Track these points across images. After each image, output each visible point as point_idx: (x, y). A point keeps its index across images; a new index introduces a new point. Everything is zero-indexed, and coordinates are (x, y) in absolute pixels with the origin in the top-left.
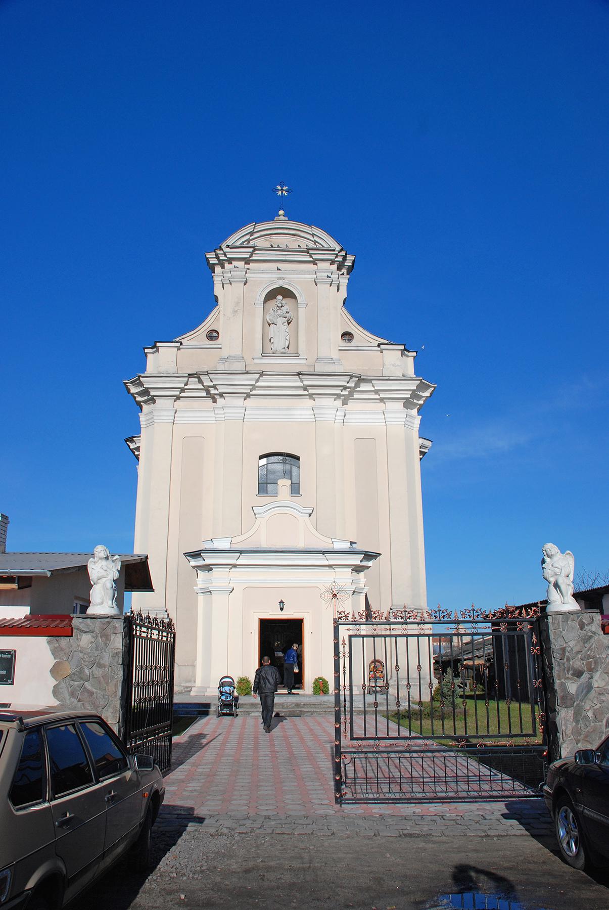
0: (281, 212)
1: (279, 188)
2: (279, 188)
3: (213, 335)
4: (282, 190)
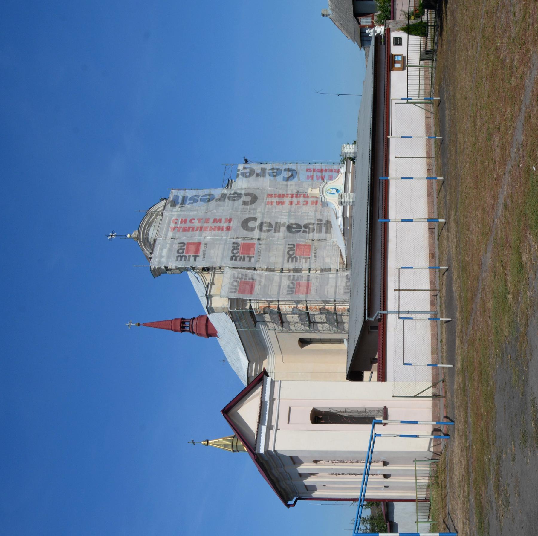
4: (112, 236)
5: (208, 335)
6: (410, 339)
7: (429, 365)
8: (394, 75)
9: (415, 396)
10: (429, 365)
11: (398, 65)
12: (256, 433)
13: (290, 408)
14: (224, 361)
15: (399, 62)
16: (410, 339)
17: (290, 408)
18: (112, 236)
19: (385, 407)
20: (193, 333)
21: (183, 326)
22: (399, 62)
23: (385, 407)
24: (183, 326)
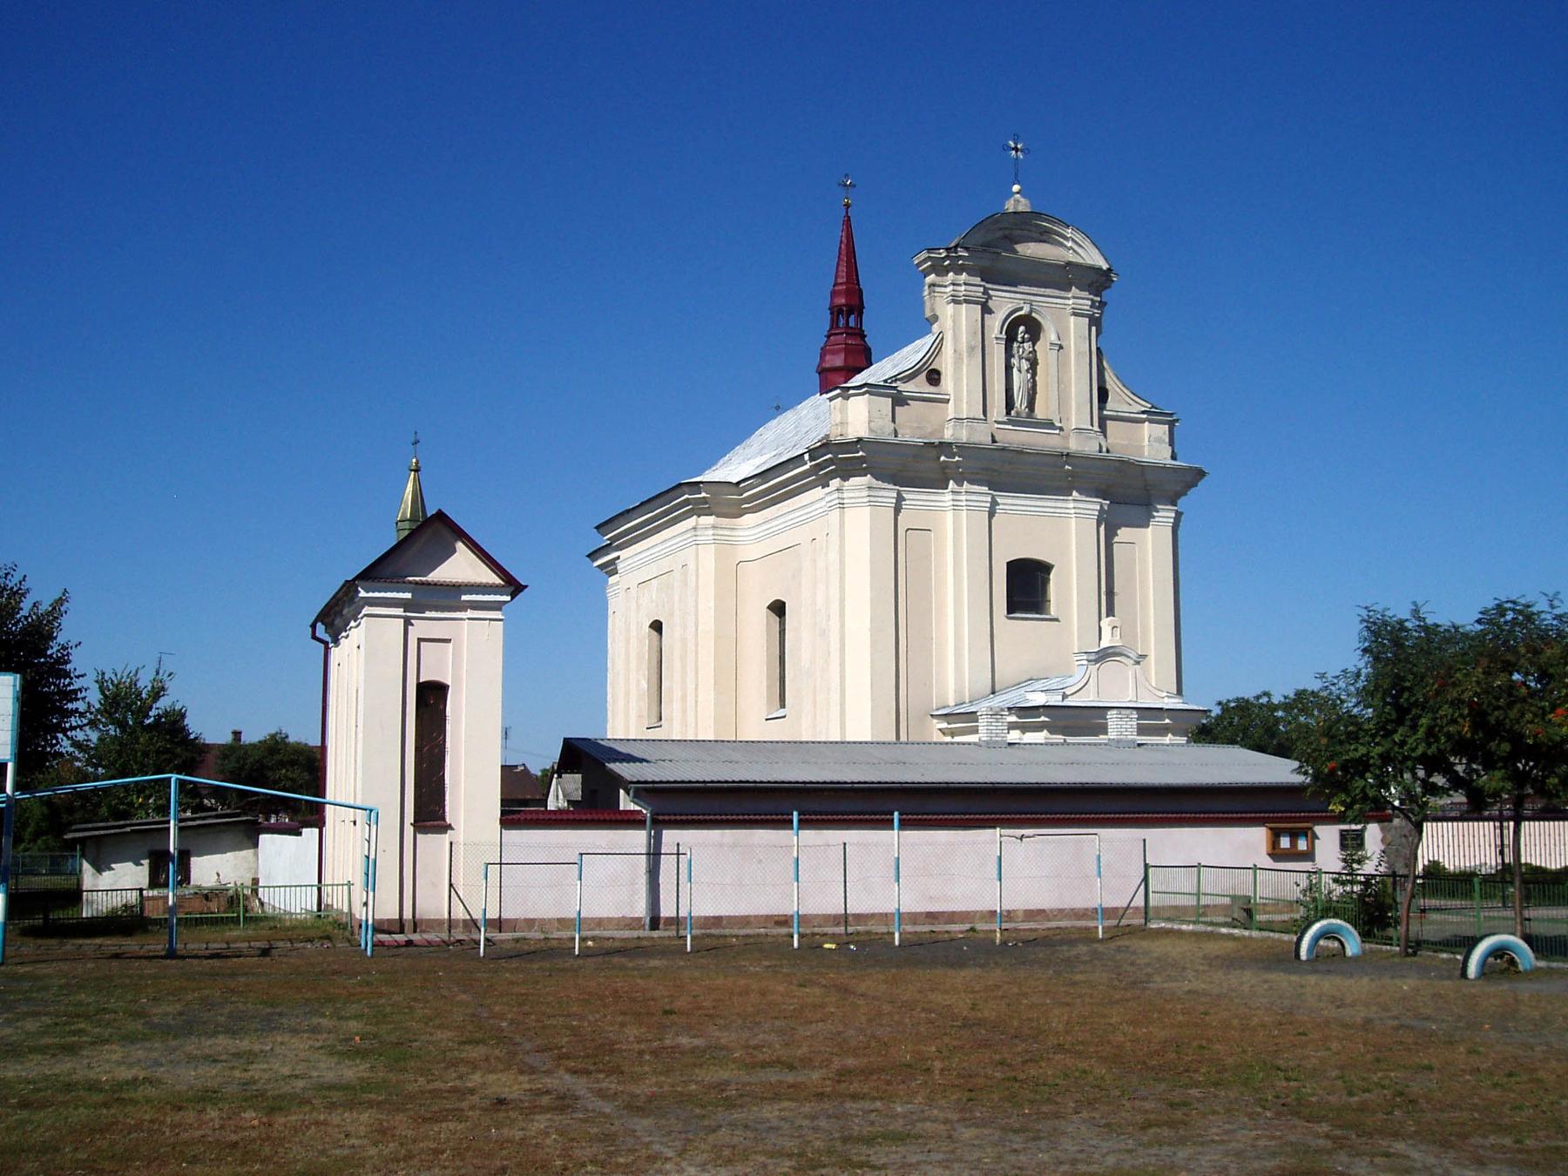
0: (1016, 188)
4: (1016, 149)
5: (823, 372)
6: (591, 880)
7: (237, 734)
8: (1257, 836)
9: (451, 885)
10: (237, 734)
11: (1285, 842)
12: (434, 576)
13: (449, 641)
14: (778, 408)
15: (1293, 844)
16: (591, 880)
17: (449, 641)
18: (1016, 149)
19: (450, 827)
20: (828, 337)
21: (849, 306)
22: (1293, 844)
23: (450, 827)
24: (849, 306)
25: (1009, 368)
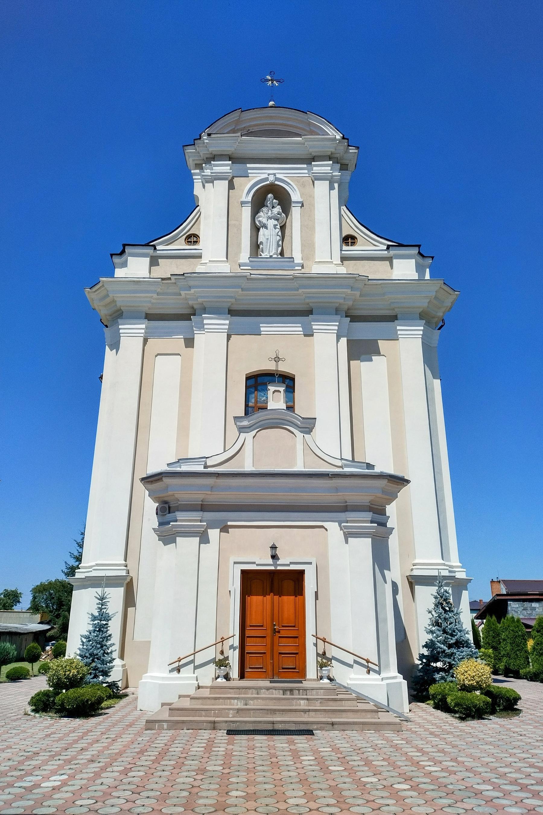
1: (269, 77)
2: (269, 77)
3: (192, 239)
25: (256, 229)
